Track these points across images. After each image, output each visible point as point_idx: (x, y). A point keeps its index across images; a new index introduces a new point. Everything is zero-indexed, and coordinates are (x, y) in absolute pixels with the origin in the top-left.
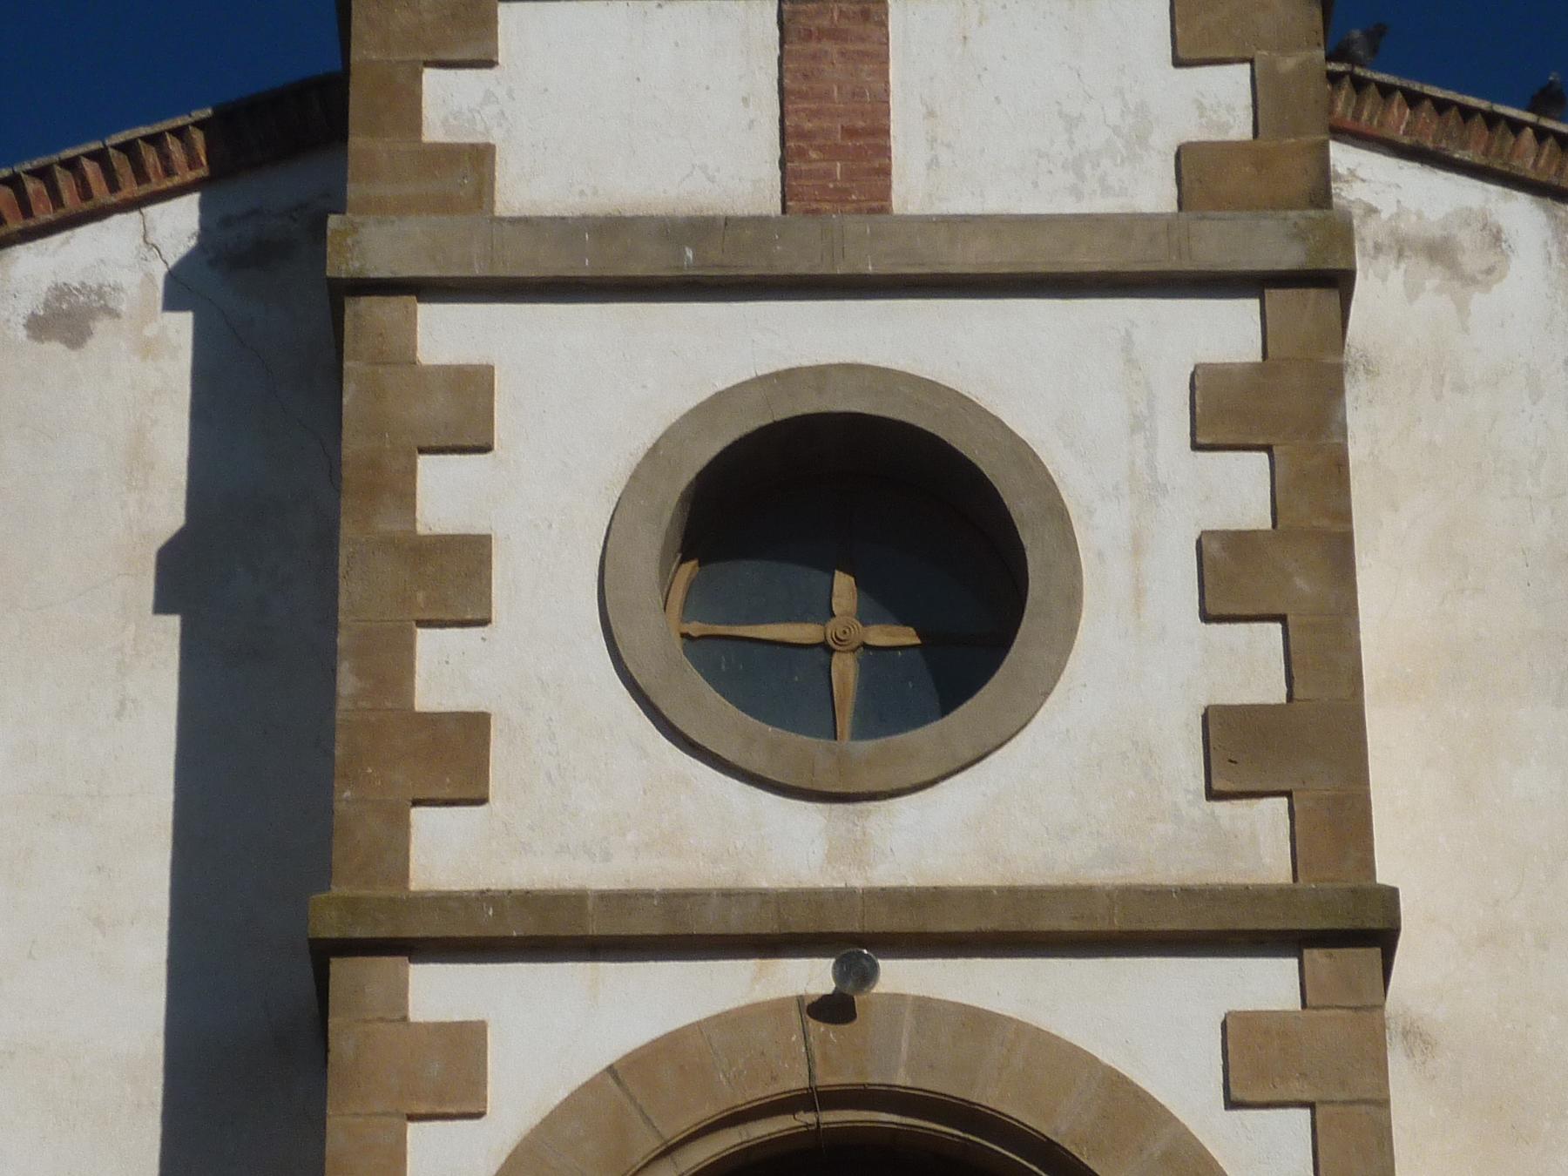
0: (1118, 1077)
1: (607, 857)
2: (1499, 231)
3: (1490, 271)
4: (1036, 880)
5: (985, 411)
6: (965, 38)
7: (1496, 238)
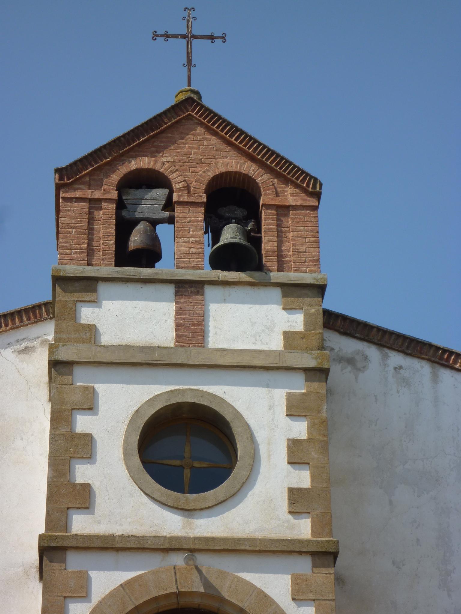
0: (261, 591)
1: (121, 525)
2: (367, 356)
3: (364, 367)
4: (240, 535)
5: (229, 403)
6: (225, 300)
7: (366, 358)
